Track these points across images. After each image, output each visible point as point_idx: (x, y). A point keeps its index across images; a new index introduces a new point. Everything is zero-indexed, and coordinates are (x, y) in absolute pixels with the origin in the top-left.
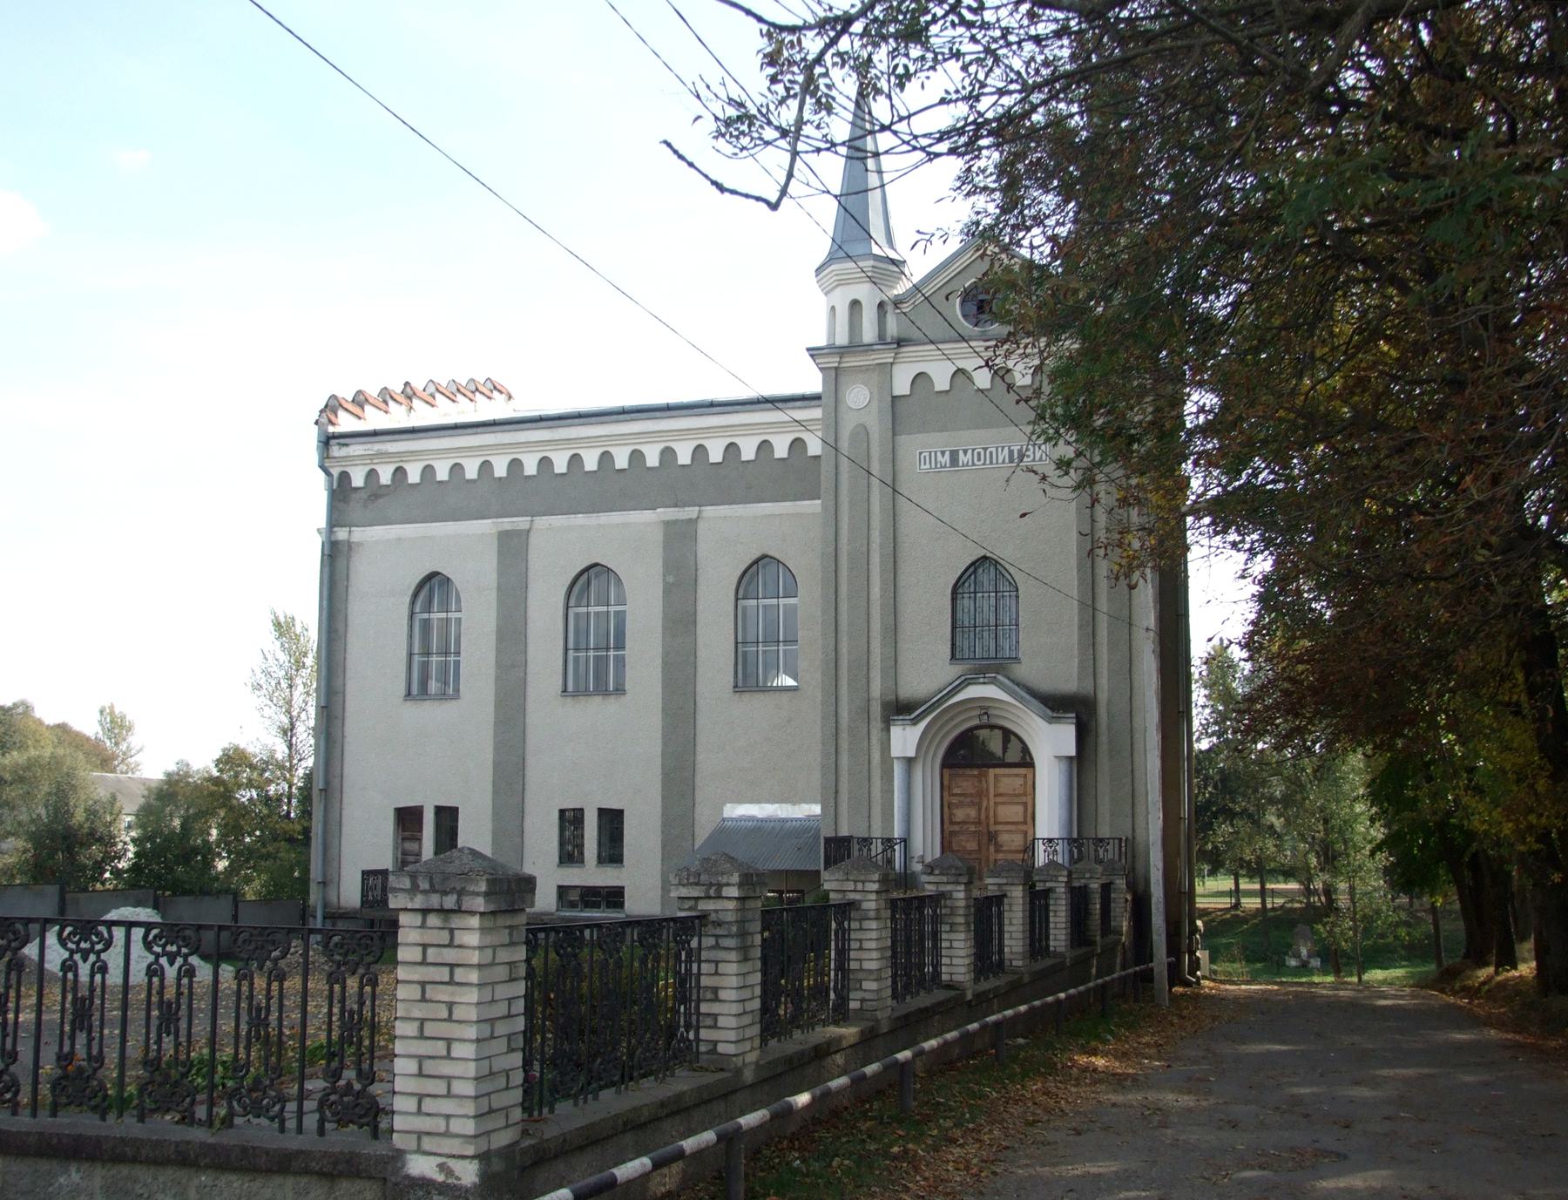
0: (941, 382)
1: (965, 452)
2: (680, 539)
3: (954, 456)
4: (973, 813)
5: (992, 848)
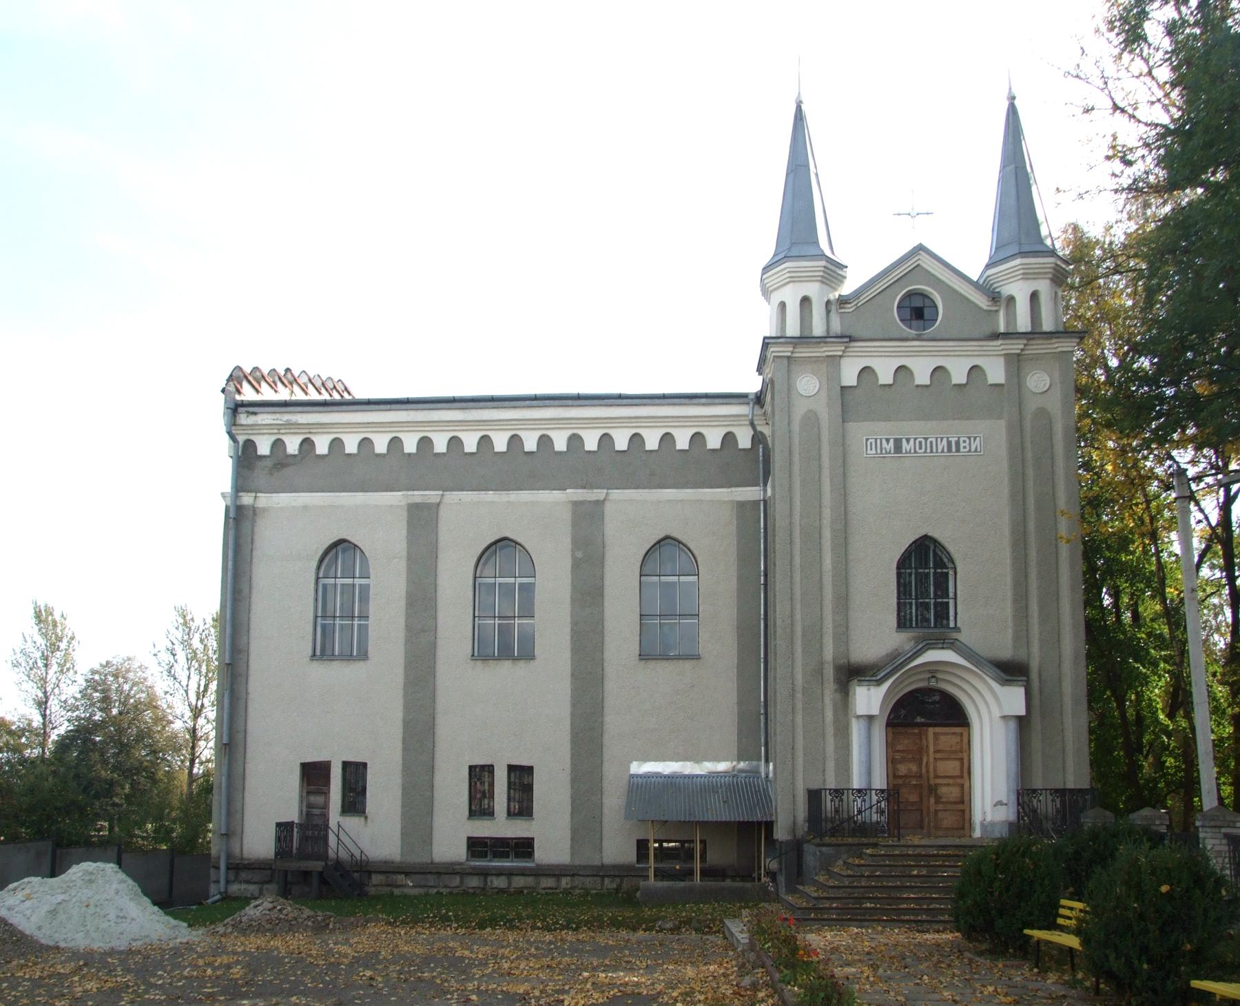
0: (885, 377)
1: (908, 440)
2: (587, 521)
3: (898, 444)
4: (914, 768)
5: (932, 800)
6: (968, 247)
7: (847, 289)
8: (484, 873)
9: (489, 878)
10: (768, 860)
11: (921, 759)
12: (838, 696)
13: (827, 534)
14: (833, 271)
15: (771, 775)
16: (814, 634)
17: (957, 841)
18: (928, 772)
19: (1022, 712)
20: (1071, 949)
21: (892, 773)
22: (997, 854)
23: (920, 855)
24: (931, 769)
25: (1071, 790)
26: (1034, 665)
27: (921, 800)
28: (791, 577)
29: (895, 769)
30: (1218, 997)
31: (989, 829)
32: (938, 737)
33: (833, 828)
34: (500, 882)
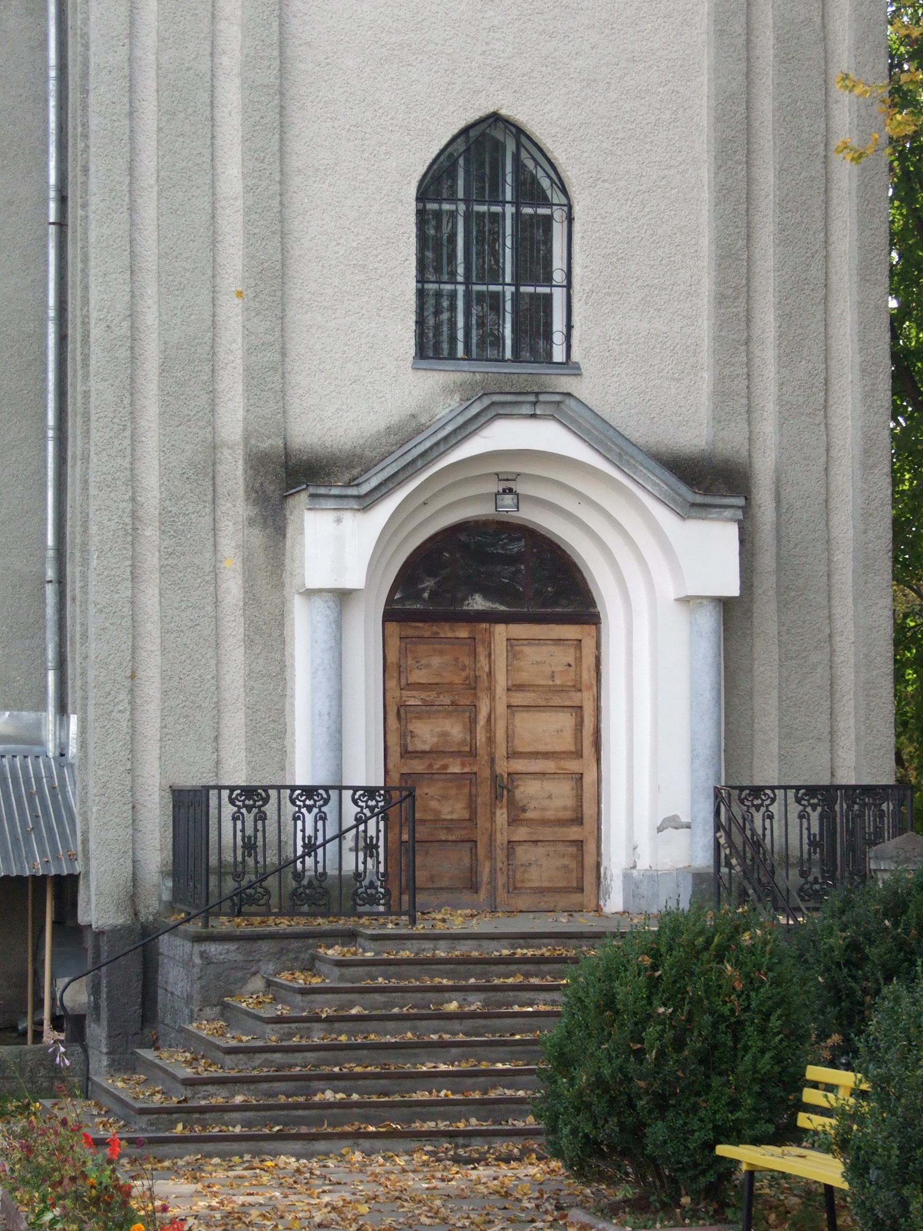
4: (456, 730)
5: (502, 816)
10: (61, 982)
11: (474, 708)
12: (257, 537)
13: (231, 95)
15: (73, 750)
16: (192, 365)
17: (562, 923)
18: (491, 741)
19: (732, 589)
20: (829, 1189)
22: (656, 955)
23: (466, 961)
24: (500, 734)
25: (850, 791)
27: (473, 818)
28: (132, 209)
29: (405, 735)
30: (744, 1167)
31: (644, 889)
32: (521, 652)
33: (238, 892)
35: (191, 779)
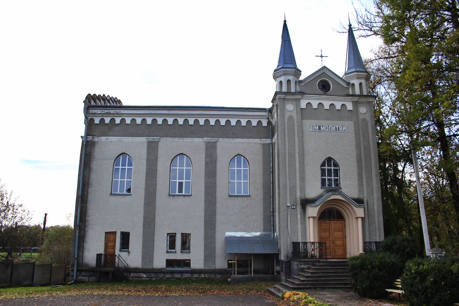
1: (323, 126)
3: (319, 127)
6: (339, 66)
7: (301, 78)
8: (172, 273)
9: (174, 274)
13: (297, 156)
14: (298, 72)
16: (293, 189)
19: (363, 216)
21: (320, 237)
26: (365, 200)
32: (334, 224)
34: (178, 276)
35: (295, 241)
